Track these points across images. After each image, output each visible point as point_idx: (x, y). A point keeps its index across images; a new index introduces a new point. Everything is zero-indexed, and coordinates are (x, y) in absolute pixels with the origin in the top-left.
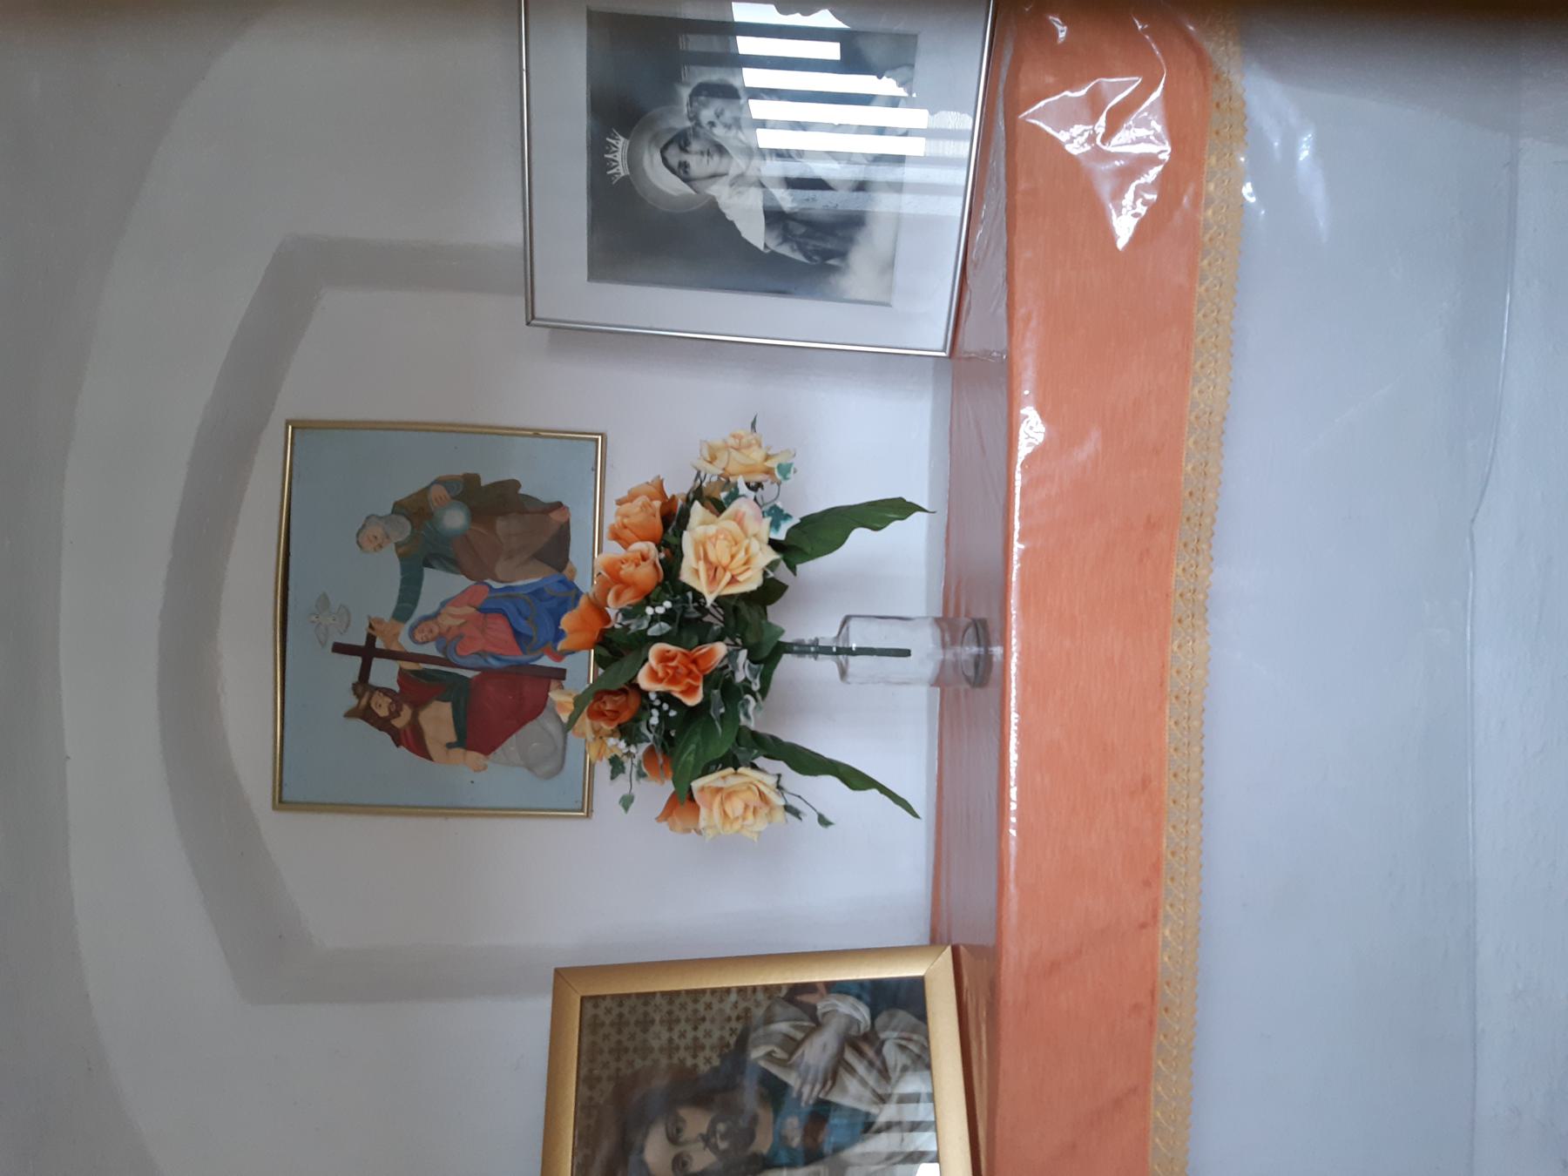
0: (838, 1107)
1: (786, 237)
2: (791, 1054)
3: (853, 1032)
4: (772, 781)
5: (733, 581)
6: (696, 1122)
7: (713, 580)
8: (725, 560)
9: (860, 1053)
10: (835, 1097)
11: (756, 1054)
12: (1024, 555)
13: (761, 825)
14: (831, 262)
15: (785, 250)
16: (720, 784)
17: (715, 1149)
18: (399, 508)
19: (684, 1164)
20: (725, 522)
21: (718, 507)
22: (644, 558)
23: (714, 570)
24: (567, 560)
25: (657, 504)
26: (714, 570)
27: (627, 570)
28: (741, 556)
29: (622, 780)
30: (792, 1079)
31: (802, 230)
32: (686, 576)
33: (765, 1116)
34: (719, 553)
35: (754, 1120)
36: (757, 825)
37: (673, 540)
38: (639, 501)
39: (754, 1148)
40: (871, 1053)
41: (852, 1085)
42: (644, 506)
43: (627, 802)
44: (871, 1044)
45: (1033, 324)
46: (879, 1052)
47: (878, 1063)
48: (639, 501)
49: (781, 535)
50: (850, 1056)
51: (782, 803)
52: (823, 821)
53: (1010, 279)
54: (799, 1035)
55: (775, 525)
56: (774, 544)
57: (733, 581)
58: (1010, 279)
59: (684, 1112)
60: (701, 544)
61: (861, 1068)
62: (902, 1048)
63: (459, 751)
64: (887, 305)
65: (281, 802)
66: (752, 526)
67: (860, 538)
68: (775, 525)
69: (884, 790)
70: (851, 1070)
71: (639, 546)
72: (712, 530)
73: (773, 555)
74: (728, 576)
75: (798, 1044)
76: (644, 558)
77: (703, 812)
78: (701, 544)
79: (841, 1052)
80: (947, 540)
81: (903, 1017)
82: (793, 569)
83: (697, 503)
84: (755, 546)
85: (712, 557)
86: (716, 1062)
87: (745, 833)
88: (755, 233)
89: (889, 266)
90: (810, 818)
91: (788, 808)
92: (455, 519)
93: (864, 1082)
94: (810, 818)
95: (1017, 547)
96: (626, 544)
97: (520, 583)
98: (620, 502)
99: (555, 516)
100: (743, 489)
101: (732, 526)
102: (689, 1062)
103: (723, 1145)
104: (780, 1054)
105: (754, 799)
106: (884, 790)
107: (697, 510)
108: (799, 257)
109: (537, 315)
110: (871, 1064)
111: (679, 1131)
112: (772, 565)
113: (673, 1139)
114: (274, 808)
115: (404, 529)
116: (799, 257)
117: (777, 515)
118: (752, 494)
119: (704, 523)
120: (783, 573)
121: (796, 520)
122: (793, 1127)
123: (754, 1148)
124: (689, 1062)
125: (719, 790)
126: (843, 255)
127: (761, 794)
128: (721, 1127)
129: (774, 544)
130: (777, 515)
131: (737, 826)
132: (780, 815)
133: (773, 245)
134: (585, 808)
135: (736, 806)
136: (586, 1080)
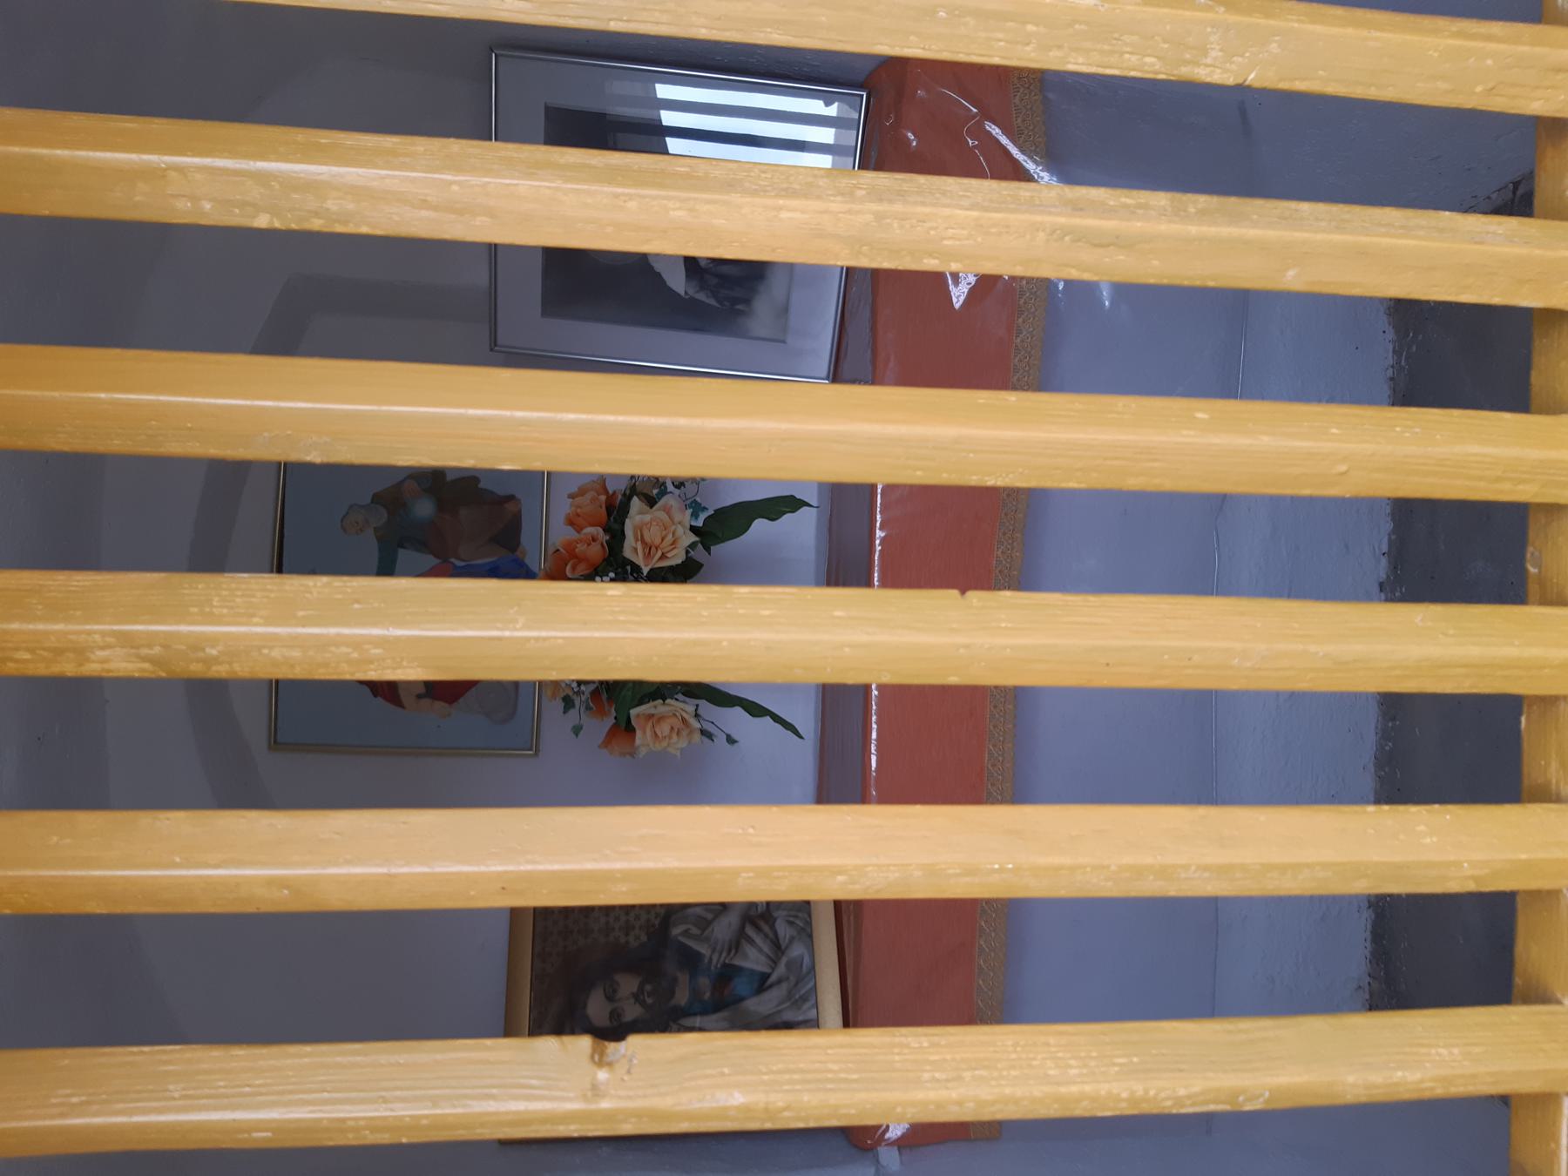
0: (740, 969)
1: (703, 287)
2: (704, 930)
3: (752, 913)
4: (691, 709)
5: (663, 557)
6: (628, 984)
7: (648, 556)
8: (657, 541)
9: (758, 929)
10: (737, 962)
11: (676, 931)
12: (883, 540)
13: (683, 743)
14: (739, 307)
15: (701, 296)
16: (653, 711)
17: (643, 1003)
18: (377, 499)
19: (619, 1016)
20: (657, 513)
21: (651, 502)
22: (594, 540)
23: (649, 549)
24: (518, 544)
25: (603, 498)
26: (649, 549)
27: (580, 548)
28: (670, 538)
29: (573, 713)
30: (704, 949)
31: (714, 281)
32: (628, 553)
33: (683, 978)
34: (653, 535)
35: (675, 980)
36: (679, 744)
37: (616, 526)
38: (589, 496)
39: (673, 1002)
40: (766, 928)
41: (751, 952)
42: (593, 500)
43: (577, 730)
44: (767, 922)
45: (891, 365)
46: (772, 927)
47: (771, 935)
48: (589, 496)
49: (700, 523)
50: (750, 931)
51: (698, 726)
52: (731, 740)
53: (874, 329)
54: (710, 916)
55: (695, 515)
56: (693, 529)
57: (663, 557)
58: (874, 329)
59: (619, 978)
60: (639, 529)
61: (758, 940)
62: (791, 923)
63: (426, 702)
64: (784, 342)
65: (276, 743)
66: (678, 517)
67: (760, 526)
68: (695, 515)
69: (777, 719)
70: (751, 941)
71: (589, 530)
72: (647, 518)
73: (693, 538)
74: (659, 554)
75: (709, 923)
76: (594, 540)
77: (639, 734)
78: (639, 529)
79: (742, 928)
80: (830, 530)
81: (637, 513)
82: (708, 549)
83: (635, 498)
84: (680, 531)
85: (647, 539)
86: (644, 938)
87: (670, 750)
88: (678, 282)
89: (784, 310)
90: (720, 739)
91: (703, 732)
92: (424, 509)
93: (761, 950)
94: (720, 739)
95: (879, 534)
96: (579, 530)
97: (480, 562)
98: (572, 496)
99: (510, 507)
100: (670, 488)
101: (663, 515)
102: (623, 940)
103: (649, 1001)
104: (695, 931)
105: (677, 724)
106: (777, 719)
107: (636, 503)
108: (712, 302)
109: (499, 342)
110: (766, 936)
111: (615, 991)
112: (693, 546)
113: (610, 998)
114: (270, 748)
115: (382, 516)
116: (712, 302)
117: (696, 508)
118: (677, 492)
119: (641, 513)
120: (699, 554)
121: (711, 512)
122: (704, 982)
123: (673, 1002)
124: (623, 940)
125: (651, 716)
126: (748, 301)
127: (684, 720)
128: (648, 987)
129: (693, 529)
130: (696, 508)
131: (664, 744)
132: (697, 737)
133: (691, 292)
134: (533, 745)
135: (664, 729)
136: (539, 956)
